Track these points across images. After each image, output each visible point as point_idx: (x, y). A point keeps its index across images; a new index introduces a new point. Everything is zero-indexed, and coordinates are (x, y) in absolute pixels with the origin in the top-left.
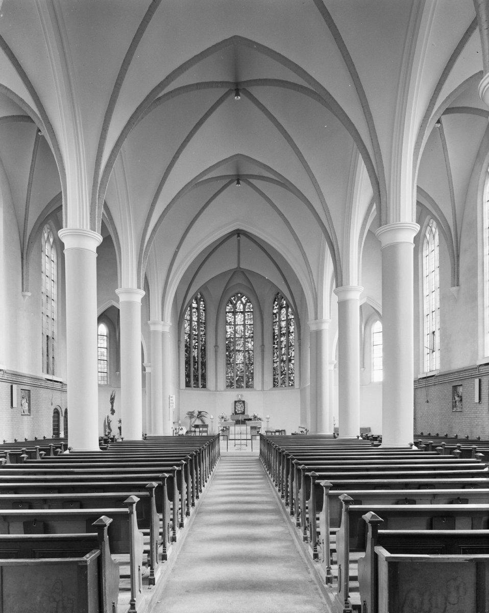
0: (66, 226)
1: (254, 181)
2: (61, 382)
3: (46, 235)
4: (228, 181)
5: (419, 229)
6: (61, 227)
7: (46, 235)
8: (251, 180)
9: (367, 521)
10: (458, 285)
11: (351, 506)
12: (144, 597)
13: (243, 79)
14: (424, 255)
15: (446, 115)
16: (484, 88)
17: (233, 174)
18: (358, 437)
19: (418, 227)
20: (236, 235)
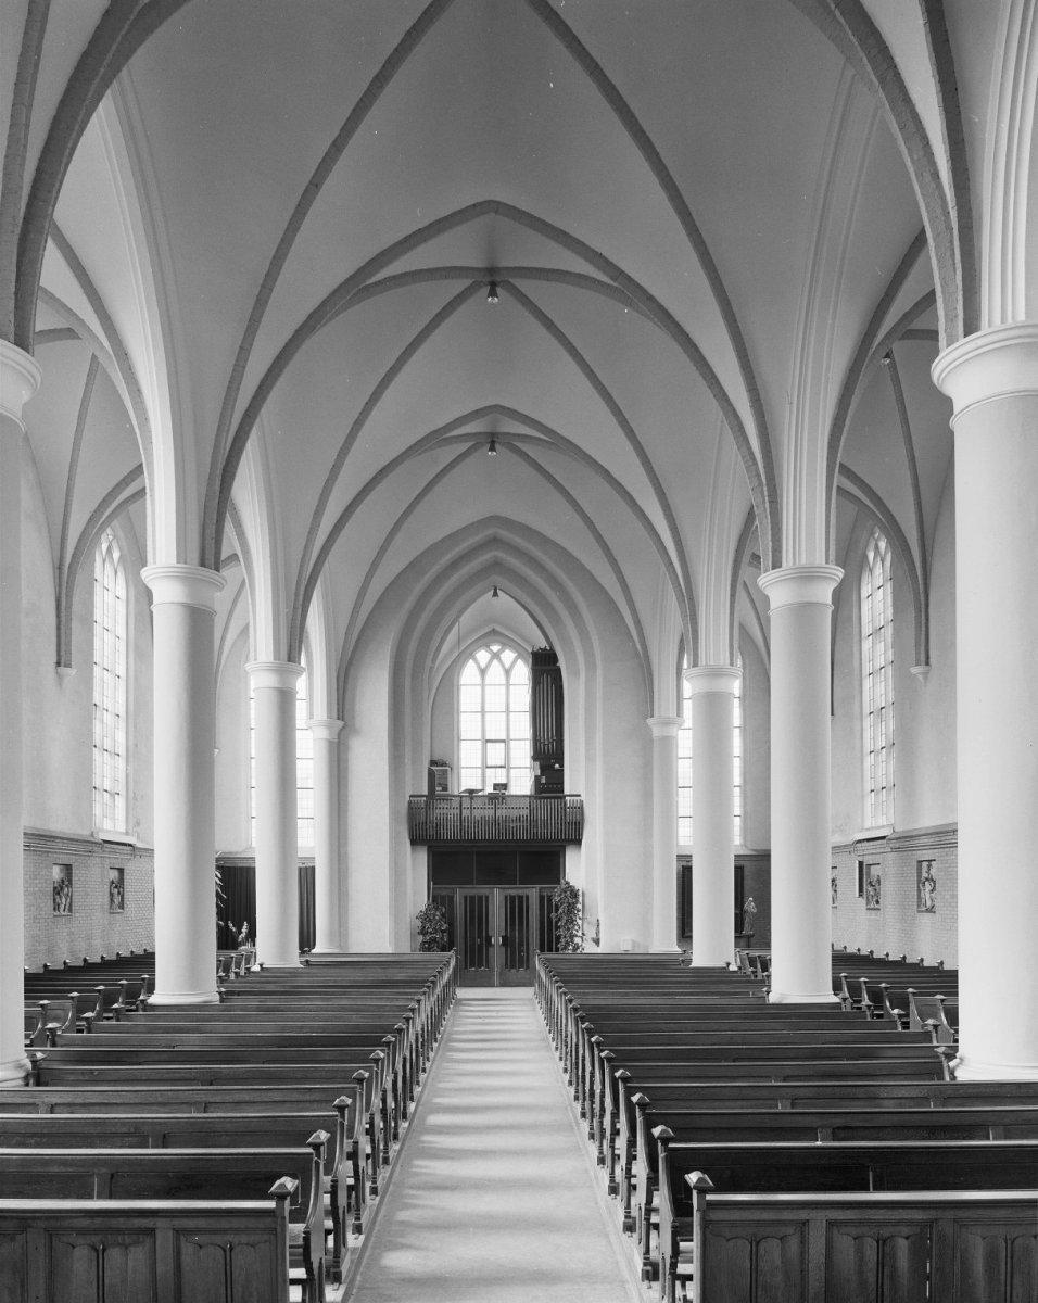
0: (155, 563)
1: (526, 286)
2: (130, 845)
3: (104, 547)
4: (467, 282)
5: (841, 576)
6: (144, 565)
7: (104, 547)
8: (518, 282)
9: (692, 1185)
10: (927, 663)
11: (671, 1145)
12: (313, 1288)
13: (504, 263)
14: (864, 593)
15: (906, 341)
16: (942, 371)
17: (480, 266)
18: (728, 964)
19: (840, 573)
20: (487, 289)
